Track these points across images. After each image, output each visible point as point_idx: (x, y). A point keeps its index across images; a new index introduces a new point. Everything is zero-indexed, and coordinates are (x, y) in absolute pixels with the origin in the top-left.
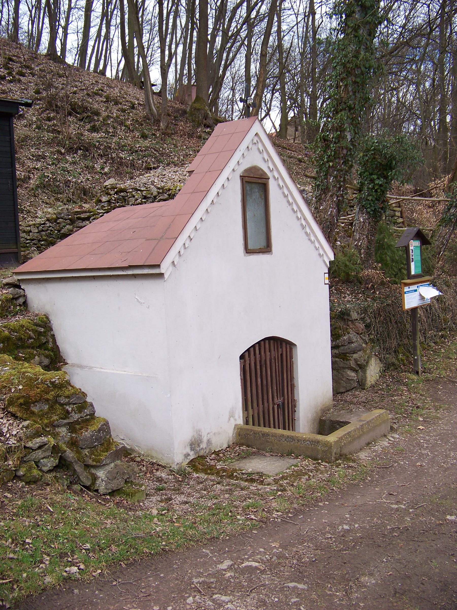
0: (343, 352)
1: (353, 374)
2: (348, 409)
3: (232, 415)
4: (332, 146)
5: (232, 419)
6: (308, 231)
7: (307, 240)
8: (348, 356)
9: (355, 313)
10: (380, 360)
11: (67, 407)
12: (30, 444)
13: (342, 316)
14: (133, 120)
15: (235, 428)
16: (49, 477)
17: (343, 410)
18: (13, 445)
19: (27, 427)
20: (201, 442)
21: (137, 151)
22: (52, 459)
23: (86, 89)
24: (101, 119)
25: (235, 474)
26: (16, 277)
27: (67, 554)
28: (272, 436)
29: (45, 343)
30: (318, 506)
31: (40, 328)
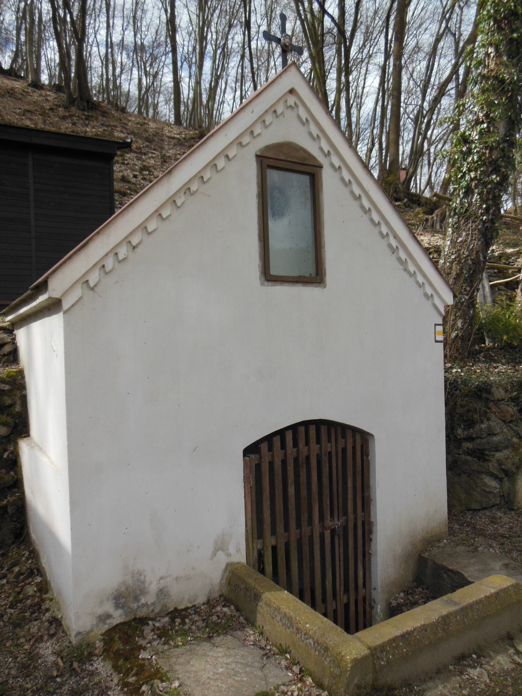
0: (479, 447)
1: (493, 483)
2: (472, 545)
5: (220, 554)
6: (403, 256)
8: (487, 455)
9: (501, 390)
13: (479, 393)
15: (226, 568)
17: (463, 544)
20: (143, 592)
31: (3, 385)
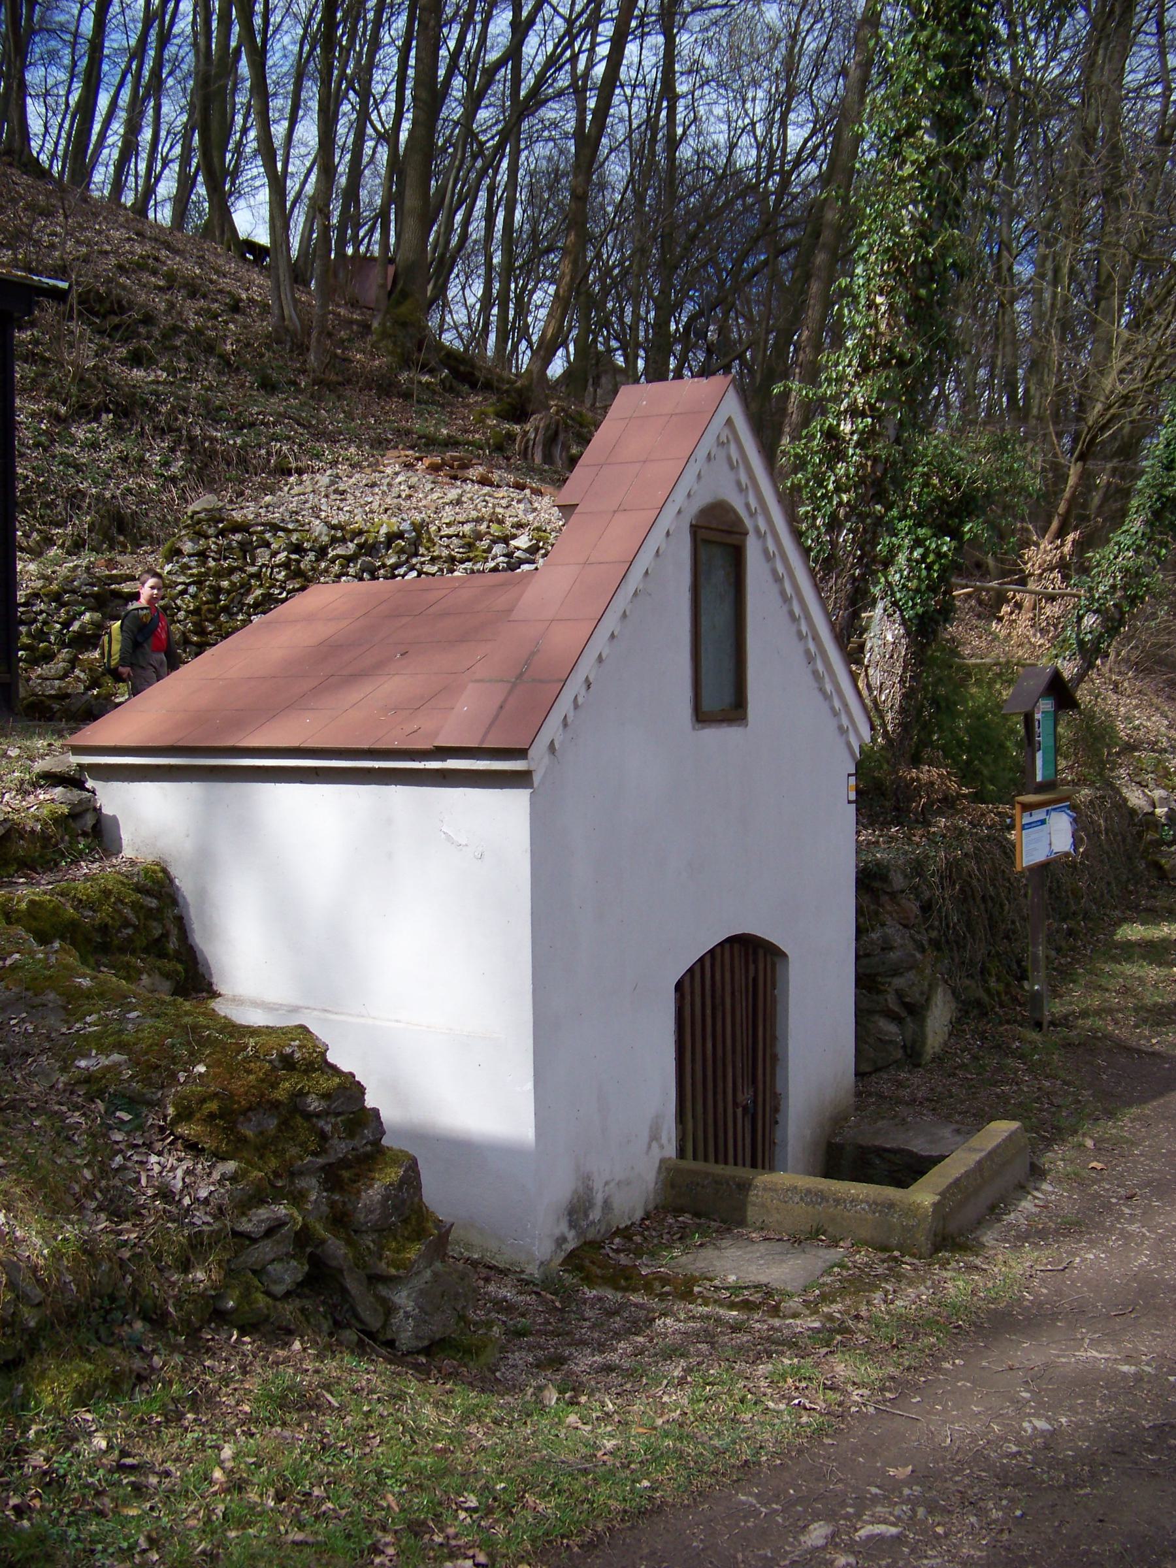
3: (654, 1137)
4: (851, 452)
5: (654, 1144)
6: (820, 668)
7: (816, 692)
10: (953, 993)
11: (321, 1123)
12: (245, 1226)
14: (238, 341)
15: (660, 1168)
16: (288, 1310)
18: (205, 1228)
19: (234, 1179)
21: (252, 425)
22: (294, 1263)
23: (115, 252)
24: (157, 333)
25: (696, 1289)
26: (75, 760)
27: (424, 1523)
28: (765, 1189)
29: (158, 940)
30: (938, 1370)
